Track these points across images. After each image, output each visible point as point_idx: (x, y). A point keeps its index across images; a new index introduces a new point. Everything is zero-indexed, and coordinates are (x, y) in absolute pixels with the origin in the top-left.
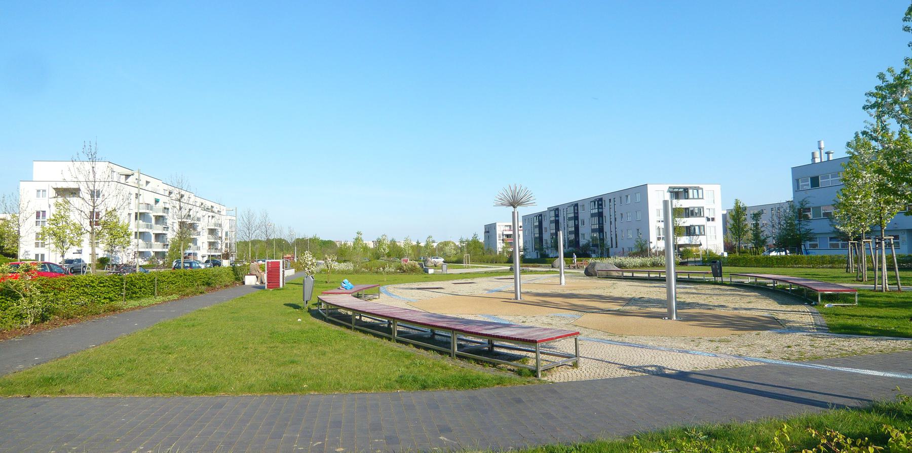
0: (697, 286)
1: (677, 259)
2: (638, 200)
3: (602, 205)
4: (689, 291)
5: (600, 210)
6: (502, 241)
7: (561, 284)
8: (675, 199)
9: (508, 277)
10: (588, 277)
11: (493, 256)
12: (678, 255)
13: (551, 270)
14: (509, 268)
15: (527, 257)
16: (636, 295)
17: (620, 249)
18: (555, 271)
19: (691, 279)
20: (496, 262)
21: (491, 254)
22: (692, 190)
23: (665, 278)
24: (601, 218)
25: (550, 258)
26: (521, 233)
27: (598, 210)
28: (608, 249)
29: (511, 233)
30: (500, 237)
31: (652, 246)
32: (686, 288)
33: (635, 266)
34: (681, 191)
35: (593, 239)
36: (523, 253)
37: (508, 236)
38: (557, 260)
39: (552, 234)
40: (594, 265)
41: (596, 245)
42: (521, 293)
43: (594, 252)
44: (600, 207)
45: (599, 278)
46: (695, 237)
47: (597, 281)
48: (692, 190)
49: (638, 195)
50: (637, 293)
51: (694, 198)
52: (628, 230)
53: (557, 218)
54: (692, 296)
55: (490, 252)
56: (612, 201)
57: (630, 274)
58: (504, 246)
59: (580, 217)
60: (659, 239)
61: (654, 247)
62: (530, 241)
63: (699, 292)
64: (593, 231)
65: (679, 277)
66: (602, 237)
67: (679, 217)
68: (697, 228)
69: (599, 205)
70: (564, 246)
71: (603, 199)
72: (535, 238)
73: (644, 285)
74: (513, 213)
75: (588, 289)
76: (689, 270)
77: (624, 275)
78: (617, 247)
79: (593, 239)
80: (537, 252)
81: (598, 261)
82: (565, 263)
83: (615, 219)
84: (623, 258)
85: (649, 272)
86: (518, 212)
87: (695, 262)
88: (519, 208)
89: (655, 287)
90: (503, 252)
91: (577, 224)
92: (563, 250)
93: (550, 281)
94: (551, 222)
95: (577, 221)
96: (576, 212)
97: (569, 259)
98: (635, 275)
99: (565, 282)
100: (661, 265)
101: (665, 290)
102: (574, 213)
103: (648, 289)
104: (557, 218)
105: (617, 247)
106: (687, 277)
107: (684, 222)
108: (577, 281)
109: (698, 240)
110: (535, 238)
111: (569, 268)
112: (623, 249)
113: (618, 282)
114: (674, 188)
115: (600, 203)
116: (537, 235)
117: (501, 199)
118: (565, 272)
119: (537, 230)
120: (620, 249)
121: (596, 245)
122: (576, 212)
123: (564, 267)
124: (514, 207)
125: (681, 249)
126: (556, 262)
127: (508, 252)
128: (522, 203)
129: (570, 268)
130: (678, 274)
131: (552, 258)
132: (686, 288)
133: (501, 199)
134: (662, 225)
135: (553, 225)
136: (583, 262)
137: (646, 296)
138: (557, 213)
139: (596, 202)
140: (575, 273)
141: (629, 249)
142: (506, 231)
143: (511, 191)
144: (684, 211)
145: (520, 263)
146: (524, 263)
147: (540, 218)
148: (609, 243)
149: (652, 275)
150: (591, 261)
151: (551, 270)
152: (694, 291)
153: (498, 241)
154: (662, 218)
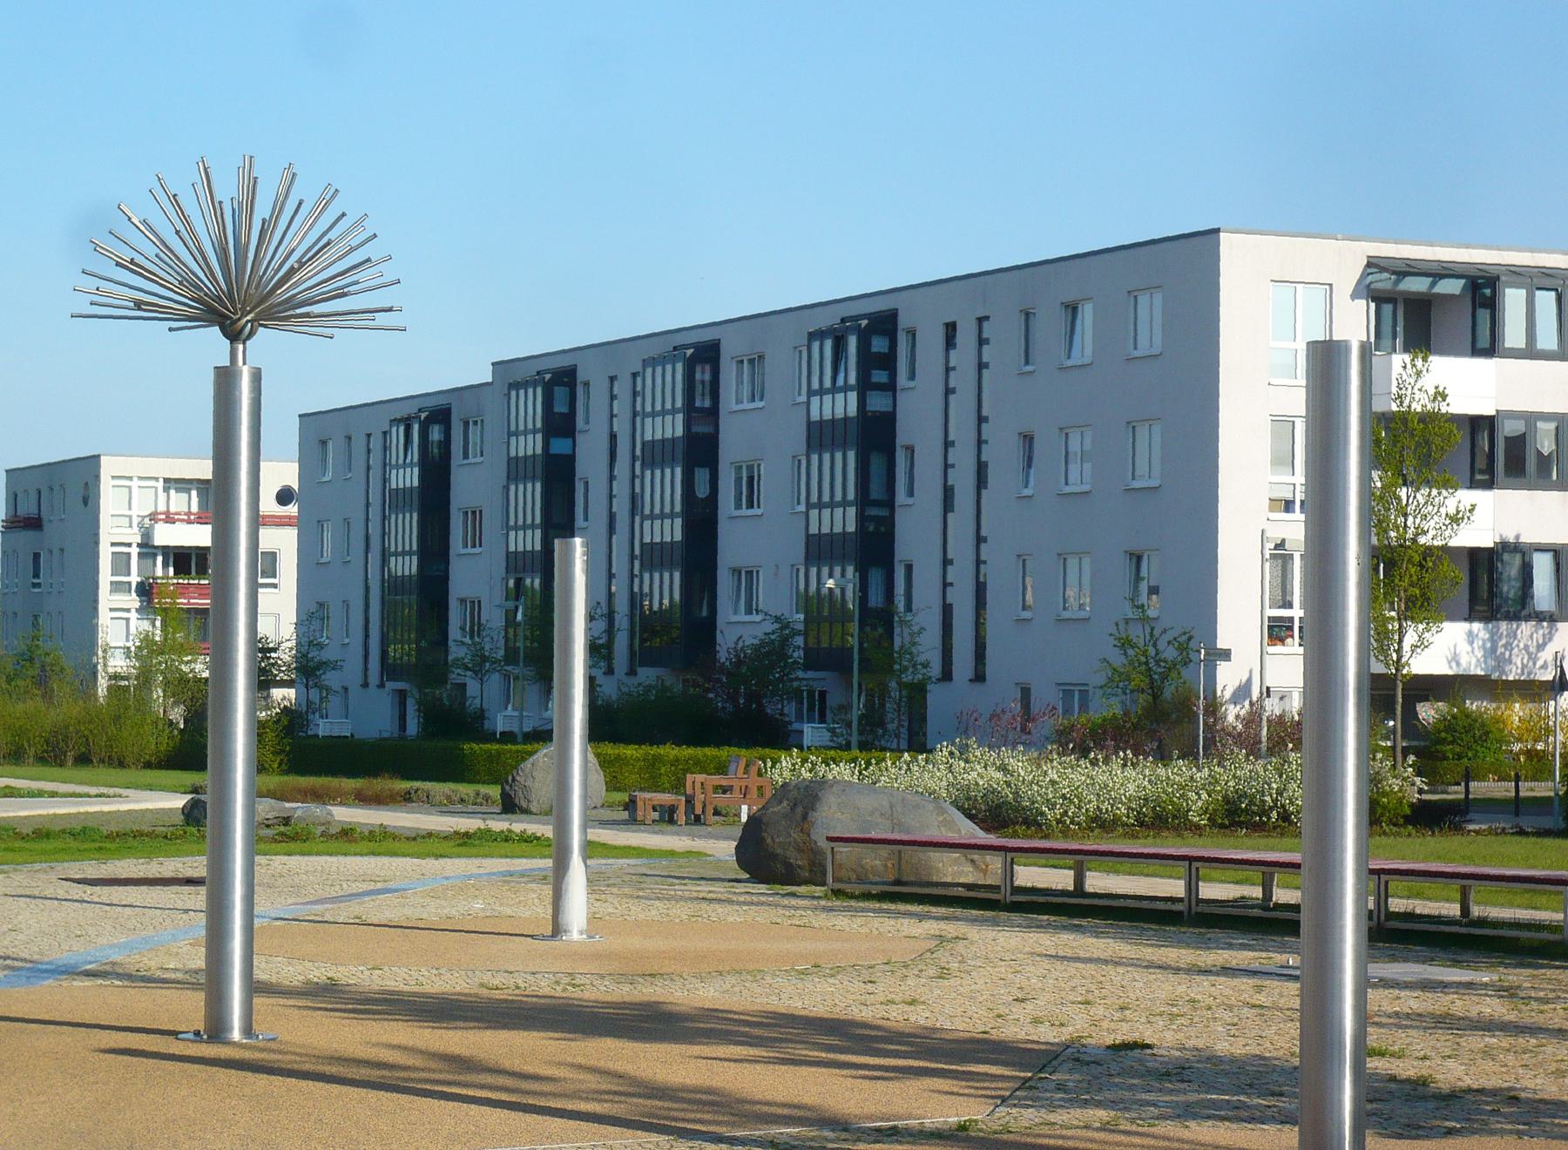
0: (1518, 976)
1: (1395, 784)
2: (1151, 337)
3: (888, 361)
4: (1458, 1005)
5: (878, 402)
6: (133, 601)
7: (557, 930)
8: (1406, 350)
9: (170, 866)
10: (762, 888)
11: (63, 711)
12: (1406, 752)
13: (499, 825)
14: (179, 802)
15: (323, 728)
16: (1095, 1024)
17: (1000, 691)
18: (525, 839)
19: (1482, 922)
20: (83, 760)
21: (48, 696)
22: (1521, 293)
23: (1296, 908)
24: (877, 463)
25: (490, 737)
26: (283, 542)
27: (688, 424)
28: (918, 692)
29: (201, 536)
30: (121, 562)
31: (1227, 678)
32: (1443, 986)
33: (1101, 823)
34: (1452, 297)
35: (817, 609)
36: (291, 693)
37: (183, 559)
38: (543, 755)
39: (517, 563)
40: (804, 799)
41: (829, 659)
42: (254, 987)
43: (819, 708)
44: (879, 376)
45: (837, 893)
46: (1526, 629)
47: (820, 920)
48: (1521, 293)
49: (1151, 309)
50: (1099, 1011)
51: (1531, 352)
52: (1063, 558)
53: (560, 446)
54: (1477, 1041)
55: (42, 681)
56: (966, 337)
57: (1061, 879)
58: (147, 640)
59: (733, 446)
60: (1277, 631)
61: (1243, 692)
62: (346, 603)
63: (1529, 1014)
64: (820, 550)
65: (1397, 905)
66: (876, 599)
67: (1429, 483)
68: (1542, 567)
69: (868, 361)
70: (598, 651)
71: (904, 322)
72: (393, 586)
73: (1149, 953)
74: (225, 379)
75: (757, 974)
76: (1470, 859)
77: (1018, 882)
78: (979, 677)
79: (817, 609)
80: (402, 696)
81: (842, 771)
82: (598, 778)
83: (981, 469)
84: (1019, 763)
85: (1194, 866)
86: (257, 376)
87: (1517, 805)
88: (267, 345)
89: (1227, 971)
90: (145, 677)
91: (702, 491)
92: (591, 682)
93: (478, 905)
94: (517, 470)
95: (701, 476)
96: (703, 402)
97: (630, 751)
98: (1099, 882)
99: (593, 918)
100: (1285, 817)
101: (1289, 994)
102: (689, 408)
103: (1181, 987)
104: (560, 446)
105: (979, 677)
106: (1453, 910)
107: (1455, 519)
108: (681, 911)
109: (1547, 655)
110: (393, 586)
111: (631, 815)
112: (1026, 692)
113: (976, 933)
114: (1406, 269)
115: (879, 345)
116: (406, 566)
117: (132, 266)
118: (590, 849)
119: (406, 529)
120: (1000, 691)
121: (829, 659)
122: (703, 402)
123: (586, 808)
124: (234, 335)
125: (1427, 712)
126: (537, 767)
127: (183, 680)
128: (291, 303)
129: (633, 821)
130: (1395, 884)
131: (508, 737)
132: (1443, 986)
133: (132, 266)
134: (1293, 528)
135: (530, 497)
136: (735, 779)
137: (1166, 1038)
138: (560, 407)
139: (852, 342)
140: (671, 854)
141: (1068, 694)
142: (170, 519)
143: (217, 208)
144: (1460, 436)
145: (259, 767)
146: (287, 772)
147: (436, 434)
148: (928, 648)
149: (1213, 890)
150: (785, 768)
151: (499, 825)
152: (1492, 1007)
153: (106, 599)
154: (1296, 481)
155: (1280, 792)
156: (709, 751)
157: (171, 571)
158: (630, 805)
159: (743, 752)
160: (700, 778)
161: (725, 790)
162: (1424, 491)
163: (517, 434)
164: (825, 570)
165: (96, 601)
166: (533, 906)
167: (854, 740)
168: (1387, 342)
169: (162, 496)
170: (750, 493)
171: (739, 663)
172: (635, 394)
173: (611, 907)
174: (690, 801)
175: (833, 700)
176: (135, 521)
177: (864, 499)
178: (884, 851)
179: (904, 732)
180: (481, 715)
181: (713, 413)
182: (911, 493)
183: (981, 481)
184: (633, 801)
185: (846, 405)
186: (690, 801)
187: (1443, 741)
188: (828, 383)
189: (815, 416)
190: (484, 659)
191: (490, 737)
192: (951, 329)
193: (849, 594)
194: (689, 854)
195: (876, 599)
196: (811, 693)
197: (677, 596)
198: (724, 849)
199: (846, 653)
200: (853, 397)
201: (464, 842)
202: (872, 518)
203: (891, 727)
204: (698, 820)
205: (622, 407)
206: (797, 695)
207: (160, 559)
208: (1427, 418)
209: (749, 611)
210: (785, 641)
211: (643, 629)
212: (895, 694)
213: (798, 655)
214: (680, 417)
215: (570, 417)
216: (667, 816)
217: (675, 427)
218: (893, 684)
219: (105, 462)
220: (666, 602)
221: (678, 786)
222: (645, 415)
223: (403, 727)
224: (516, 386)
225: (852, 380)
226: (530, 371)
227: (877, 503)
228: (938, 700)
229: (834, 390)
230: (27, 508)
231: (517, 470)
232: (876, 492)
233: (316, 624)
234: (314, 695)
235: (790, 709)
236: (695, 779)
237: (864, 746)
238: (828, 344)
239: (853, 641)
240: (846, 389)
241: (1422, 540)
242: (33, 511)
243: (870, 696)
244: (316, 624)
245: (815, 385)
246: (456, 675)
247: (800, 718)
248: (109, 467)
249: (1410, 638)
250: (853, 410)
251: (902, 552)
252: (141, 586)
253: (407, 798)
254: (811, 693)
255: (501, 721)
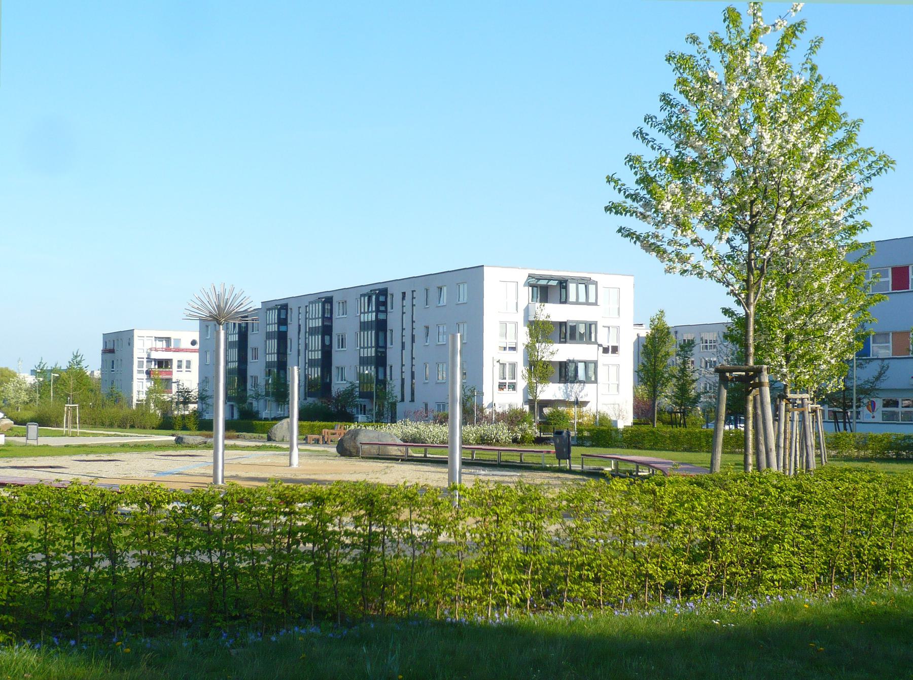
3: (385, 304)
5: (381, 316)
6: (145, 376)
7: (290, 465)
8: (541, 302)
11: (125, 412)
13: (268, 444)
14: (174, 438)
17: (419, 404)
20: (132, 427)
22: (574, 285)
24: (381, 334)
25: (261, 420)
28: (393, 405)
30: (141, 364)
31: (486, 401)
36: (196, 406)
40: (355, 433)
43: (363, 410)
44: (382, 308)
46: (576, 385)
47: (357, 463)
48: (574, 285)
49: (464, 289)
51: (577, 303)
53: (283, 328)
64: (364, 361)
66: (381, 377)
68: (581, 367)
78: (412, 400)
80: (232, 406)
83: (413, 337)
84: (422, 426)
90: (148, 401)
91: (327, 343)
93: (269, 460)
94: (269, 336)
95: (327, 338)
99: (300, 464)
104: (283, 328)
105: (412, 400)
107: (552, 353)
112: (426, 405)
115: (382, 299)
122: (327, 315)
125: (546, 411)
131: (266, 419)
138: (283, 316)
139: (374, 297)
140: (319, 451)
142: (156, 350)
148: (397, 391)
153: (136, 375)
155: (496, 434)
156: (330, 423)
157: (157, 367)
158: (306, 439)
159: (340, 423)
160: (327, 430)
161: (334, 434)
162: (544, 344)
163: (269, 324)
164: (365, 368)
165: (132, 376)
166: (284, 460)
167: (374, 420)
168: (535, 299)
169: (154, 342)
170: (342, 343)
171: (339, 396)
172: (306, 312)
173: (303, 461)
174: (323, 437)
175: (367, 408)
176: (145, 351)
177: (377, 346)
178: (376, 447)
179: (390, 418)
180: (257, 413)
181: (331, 319)
182: (392, 344)
183: (413, 341)
184: (307, 437)
185: (372, 317)
186: (323, 437)
187: (551, 420)
188: (366, 310)
189: (362, 320)
190: (259, 395)
191: (848, 389)
192: (404, 294)
193: (373, 374)
194: (323, 451)
195: (381, 377)
196: (361, 405)
197: (319, 374)
198: (334, 450)
199: (371, 393)
200: (374, 314)
201: (258, 448)
202: (380, 352)
203: (386, 416)
204: (326, 443)
205: (302, 317)
206: (357, 406)
207: (153, 363)
208: (544, 323)
209: (342, 380)
210: (352, 390)
211: (309, 386)
212: (386, 406)
213: (357, 394)
214: (320, 320)
215: (286, 319)
216: (317, 442)
217: (318, 323)
218: (386, 403)
219: (135, 332)
220: (316, 376)
221: (320, 433)
222: (309, 319)
223: (233, 416)
224: (269, 309)
225: (374, 309)
226: (273, 305)
227: (381, 347)
228: (400, 407)
229: (368, 312)
230: (110, 347)
231: (269, 336)
232: (381, 343)
233: (205, 384)
234: (204, 406)
235: (354, 410)
236: (325, 431)
237: (377, 422)
238: (366, 298)
239: (374, 390)
240: (372, 312)
241: (543, 359)
242: (112, 347)
243: (379, 406)
244: (205, 384)
245: (363, 311)
246: (249, 400)
247: (358, 413)
248: (136, 333)
249: (539, 389)
250: (374, 318)
251: (389, 362)
252: (147, 371)
253: (238, 437)
254: (361, 405)
255: (264, 415)
